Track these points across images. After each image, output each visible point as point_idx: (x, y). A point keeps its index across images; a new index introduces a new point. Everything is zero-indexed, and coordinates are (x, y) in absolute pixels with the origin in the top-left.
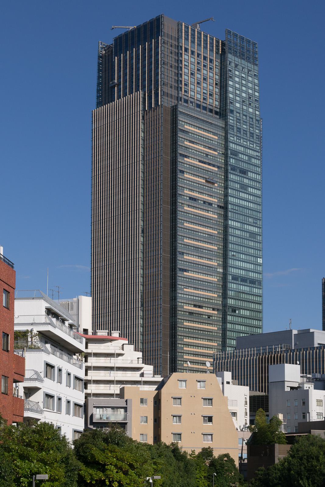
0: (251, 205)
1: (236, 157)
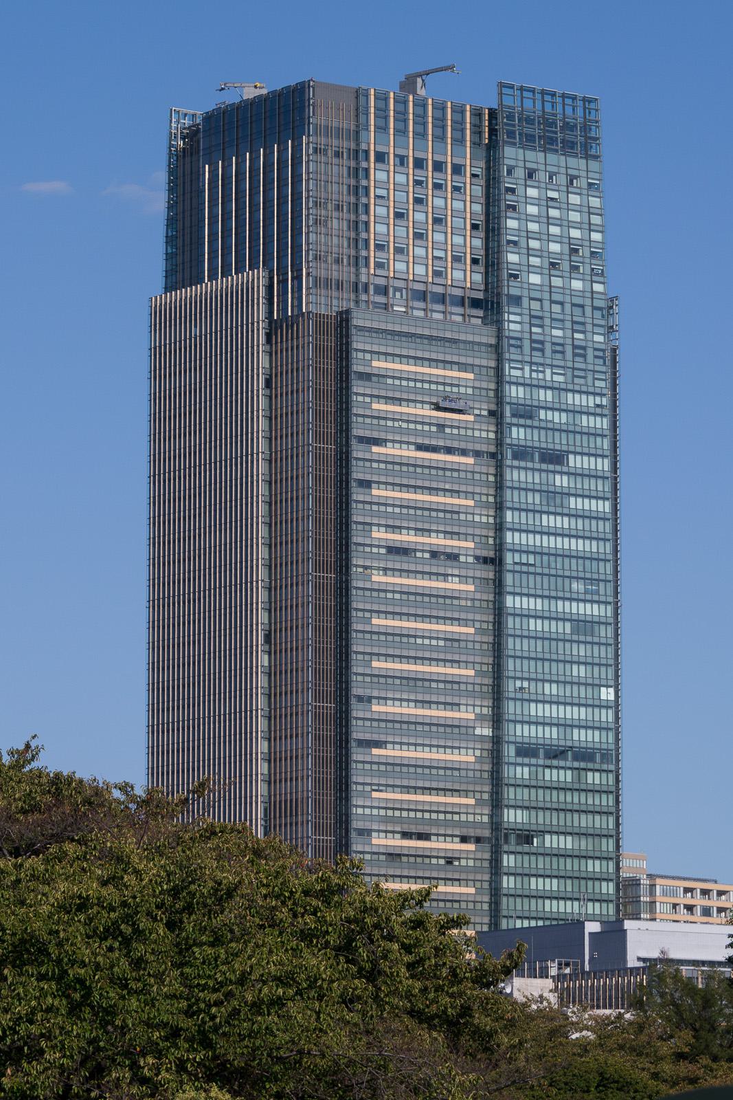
0: (579, 545)
1: (529, 422)
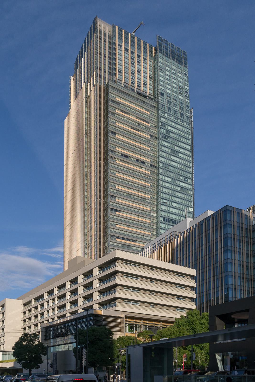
0: (181, 166)
